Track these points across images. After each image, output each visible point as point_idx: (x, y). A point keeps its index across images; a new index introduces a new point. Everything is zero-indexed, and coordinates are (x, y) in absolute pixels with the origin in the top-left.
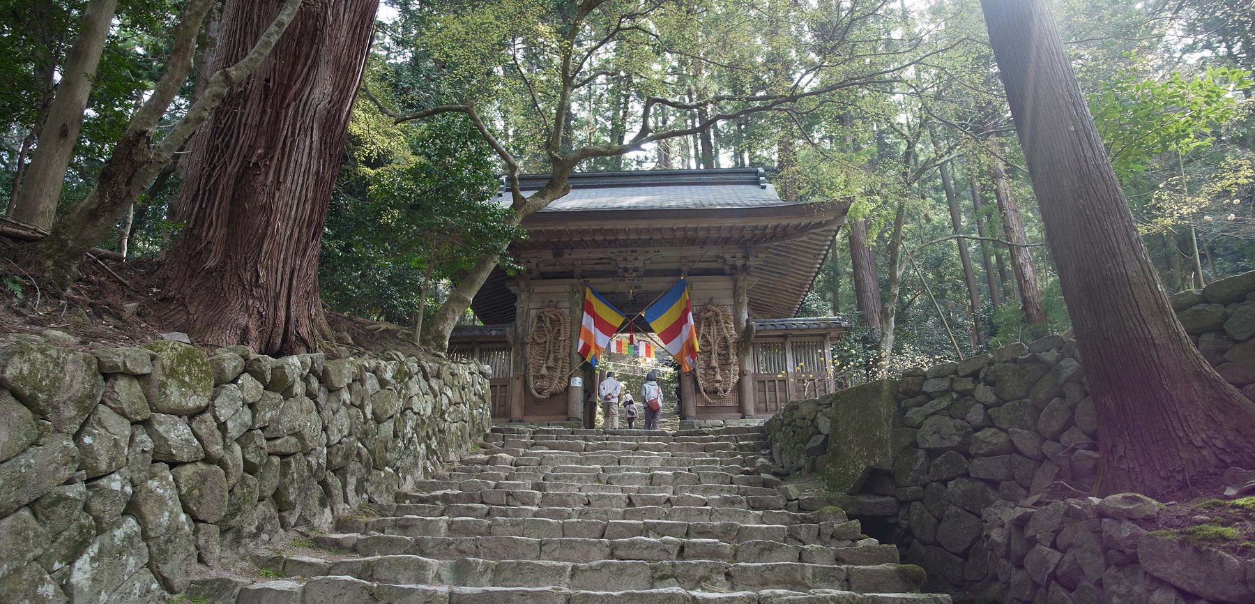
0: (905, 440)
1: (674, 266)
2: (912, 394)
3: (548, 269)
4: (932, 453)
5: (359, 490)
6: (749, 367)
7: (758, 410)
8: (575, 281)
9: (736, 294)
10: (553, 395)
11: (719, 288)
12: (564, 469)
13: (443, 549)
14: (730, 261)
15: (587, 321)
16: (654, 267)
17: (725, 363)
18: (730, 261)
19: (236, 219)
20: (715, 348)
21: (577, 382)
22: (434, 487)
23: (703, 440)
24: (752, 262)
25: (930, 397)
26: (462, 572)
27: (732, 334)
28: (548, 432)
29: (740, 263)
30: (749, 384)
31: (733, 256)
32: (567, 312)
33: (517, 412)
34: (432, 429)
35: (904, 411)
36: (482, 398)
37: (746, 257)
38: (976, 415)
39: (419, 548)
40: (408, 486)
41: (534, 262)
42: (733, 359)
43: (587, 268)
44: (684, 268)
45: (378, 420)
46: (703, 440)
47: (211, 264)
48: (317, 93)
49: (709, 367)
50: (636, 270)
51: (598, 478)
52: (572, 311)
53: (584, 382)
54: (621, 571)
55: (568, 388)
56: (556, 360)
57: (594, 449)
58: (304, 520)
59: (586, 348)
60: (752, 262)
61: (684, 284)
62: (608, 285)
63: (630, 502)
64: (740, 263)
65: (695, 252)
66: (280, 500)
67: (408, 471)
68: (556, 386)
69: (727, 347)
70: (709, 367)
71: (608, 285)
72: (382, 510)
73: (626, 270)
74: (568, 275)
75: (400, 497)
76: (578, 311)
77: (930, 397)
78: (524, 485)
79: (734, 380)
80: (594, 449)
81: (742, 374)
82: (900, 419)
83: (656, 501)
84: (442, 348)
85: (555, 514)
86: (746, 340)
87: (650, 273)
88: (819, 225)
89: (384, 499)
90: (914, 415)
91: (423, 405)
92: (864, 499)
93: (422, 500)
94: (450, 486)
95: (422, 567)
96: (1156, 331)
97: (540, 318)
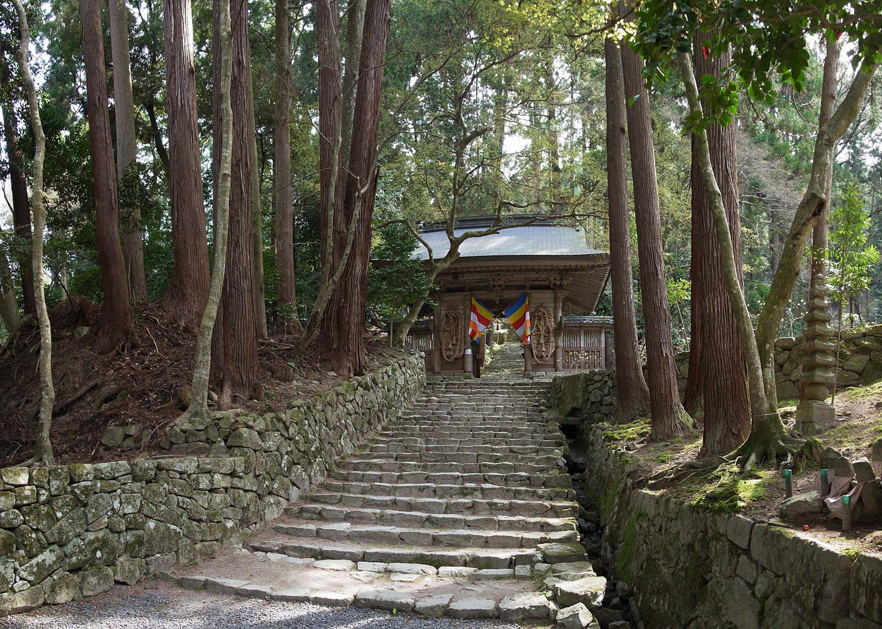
0: (586, 397)
1: (523, 283)
2: (591, 380)
3: (451, 286)
4: (593, 403)
5: (387, 417)
6: (561, 344)
7: (564, 367)
8: (466, 293)
9: (556, 301)
10: (456, 359)
11: (546, 296)
12: (460, 405)
13: (420, 436)
14: (553, 281)
15: (473, 317)
16: (511, 284)
17: (547, 342)
18: (553, 281)
19: (339, 328)
20: (543, 333)
21: (469, 352)
22: (409, 414)
23: (525, 389)
24: (565, 282)
25: (596, 382)
26: (427, 442)
27: (552, 325)
28: (453, 384)
29: (558, 283)
30: (560, 353)
31: (554, 279)
32: (462, 311)
33: (437, 369)
34: (405, 389)
35: (588, 386)
36: (421, 369)
37: (562, 279)
38: (606, 391)
39: (412, 435)
40: (400, 414)
41: (442, 282)
42: (552, 339)
43: (473, 284)
44: (527, 285)
45: (389, 391)
46: (525, 389)
47: (335, 346)
48: (357, 270)
49: (539, 343)
50: (500, 286)
51: (474, 409)
52: (465, 311)
53: (473, 352)
54: (474, 441)
55: (464, 355)
56: (457, 340)
57: (474, 393)
58: (375, 428)
59: (474, 333)
60: (565, 282)
61: (526, 295)
62: (484, 295)
63: (484, 420)
64: (558, 283)
65: (533, 276)
66: (369, 423)
67: (399, 408)
68: (457, 354)
69: (549, 332)
70: (539, 343)
71: (484, 295)
72: (394, 423)
73: (494, 286)
74: (461, 289)
75: (398, 418)
76: (468, 311)
77: (596, 382)
78: (443, 412)
79: (552, 350)
80: (474, 393)
81: (557, 347)
82: (586, 391)
83: (493, 419)
84: (402, 347)
85: (455, 424)
86: (559, 329)
87: (508, 288)
88: (599, 266)
89: (394, 419)
90: (590, 388)
91: (401, 381)
92: (570, 418)
93: (406, 419)
94: (415, 413)
95: (416, 440)
96: (633, 376)
97: (447, 316)
